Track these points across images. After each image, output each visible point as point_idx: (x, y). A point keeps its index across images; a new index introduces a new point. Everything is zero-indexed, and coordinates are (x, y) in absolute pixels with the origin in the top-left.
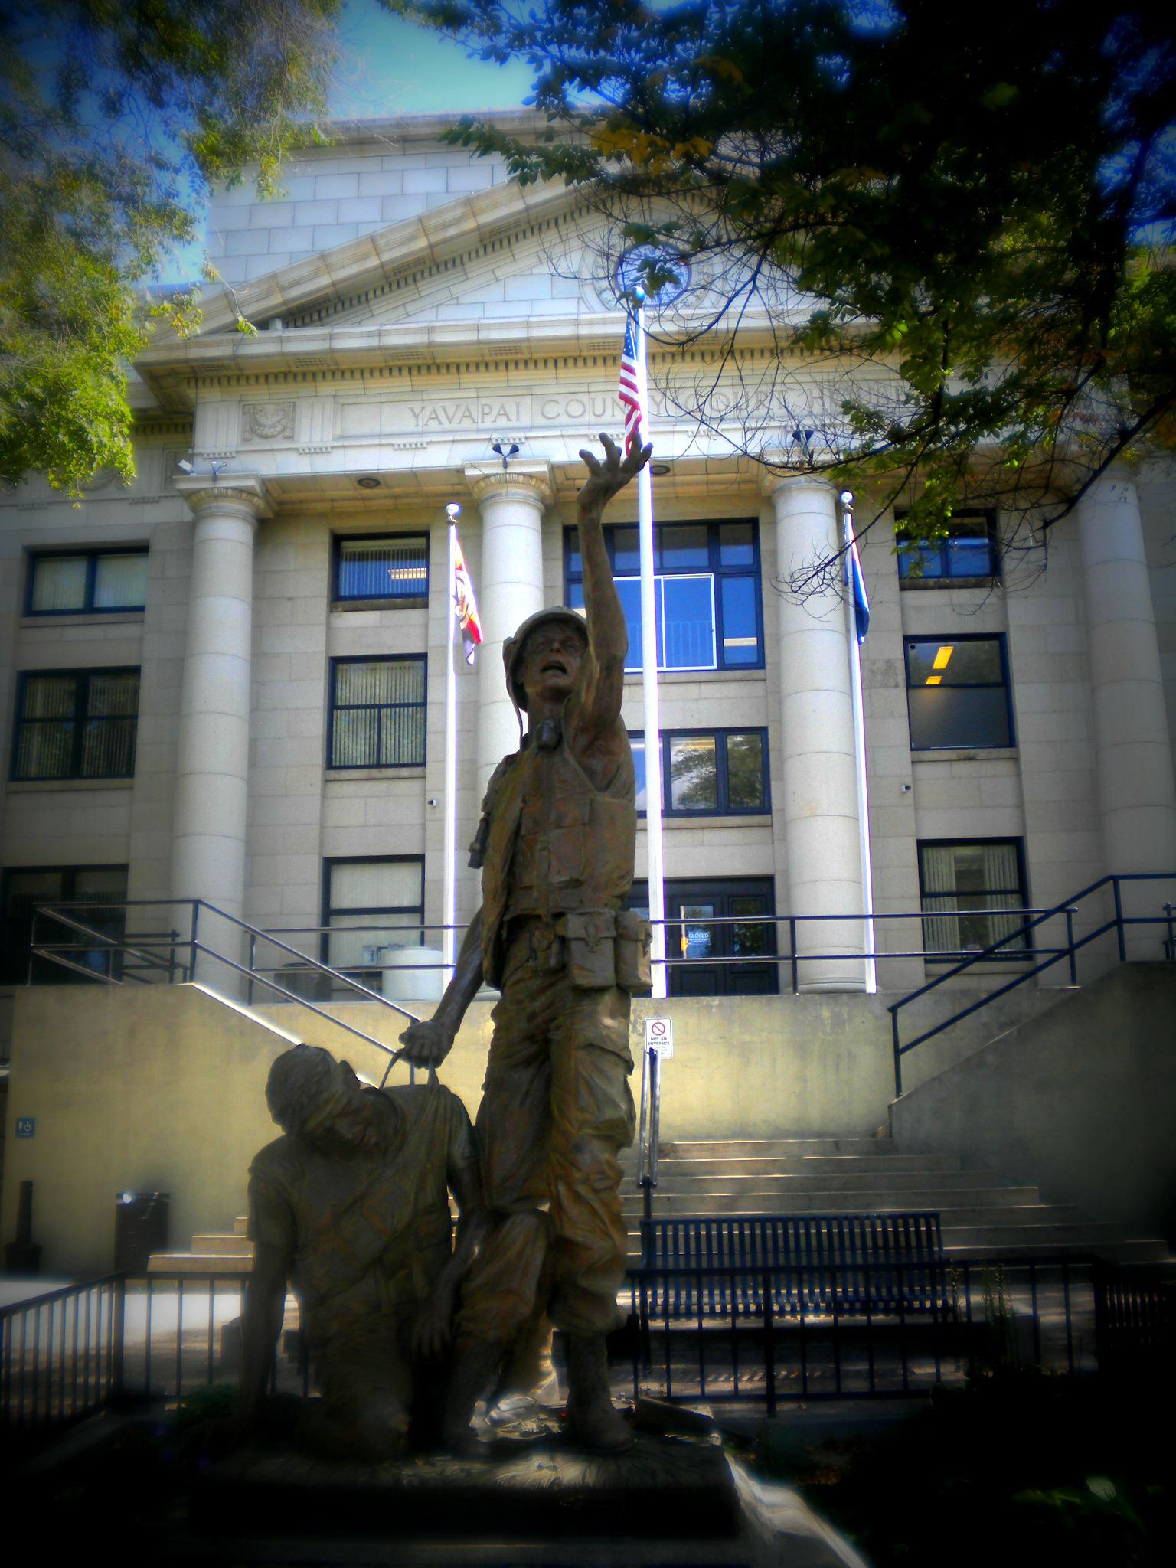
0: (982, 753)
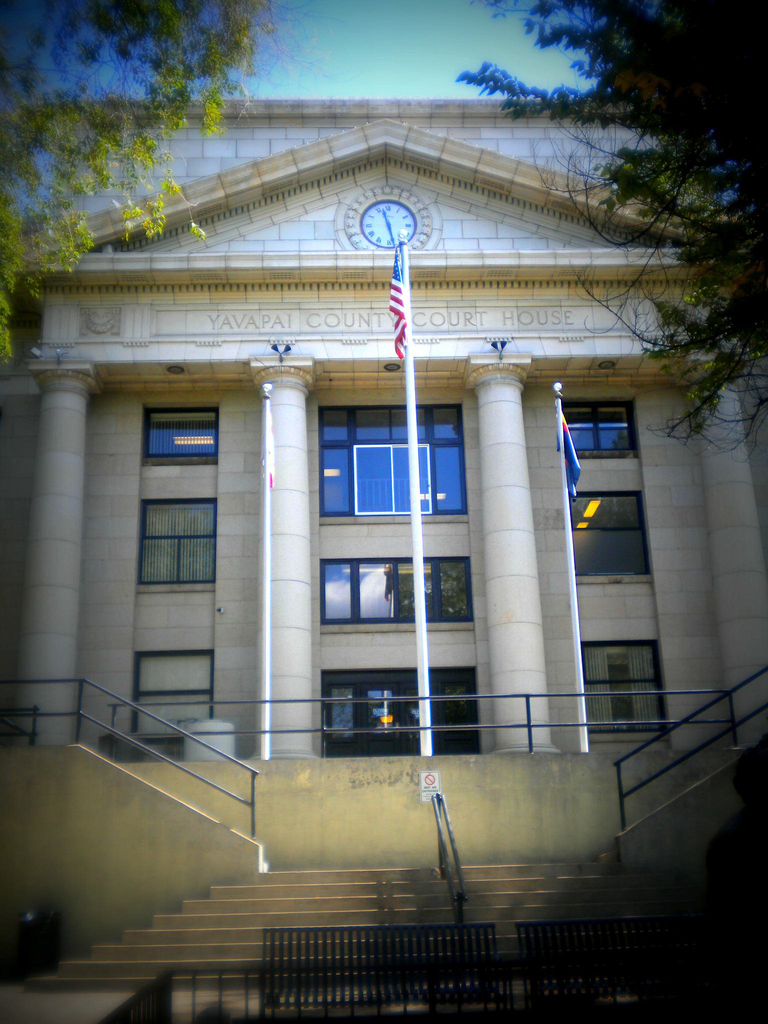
0: (626, 578)
